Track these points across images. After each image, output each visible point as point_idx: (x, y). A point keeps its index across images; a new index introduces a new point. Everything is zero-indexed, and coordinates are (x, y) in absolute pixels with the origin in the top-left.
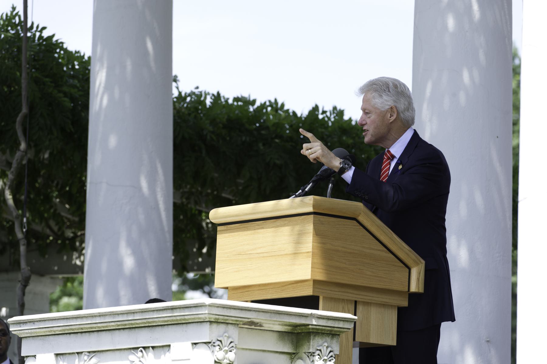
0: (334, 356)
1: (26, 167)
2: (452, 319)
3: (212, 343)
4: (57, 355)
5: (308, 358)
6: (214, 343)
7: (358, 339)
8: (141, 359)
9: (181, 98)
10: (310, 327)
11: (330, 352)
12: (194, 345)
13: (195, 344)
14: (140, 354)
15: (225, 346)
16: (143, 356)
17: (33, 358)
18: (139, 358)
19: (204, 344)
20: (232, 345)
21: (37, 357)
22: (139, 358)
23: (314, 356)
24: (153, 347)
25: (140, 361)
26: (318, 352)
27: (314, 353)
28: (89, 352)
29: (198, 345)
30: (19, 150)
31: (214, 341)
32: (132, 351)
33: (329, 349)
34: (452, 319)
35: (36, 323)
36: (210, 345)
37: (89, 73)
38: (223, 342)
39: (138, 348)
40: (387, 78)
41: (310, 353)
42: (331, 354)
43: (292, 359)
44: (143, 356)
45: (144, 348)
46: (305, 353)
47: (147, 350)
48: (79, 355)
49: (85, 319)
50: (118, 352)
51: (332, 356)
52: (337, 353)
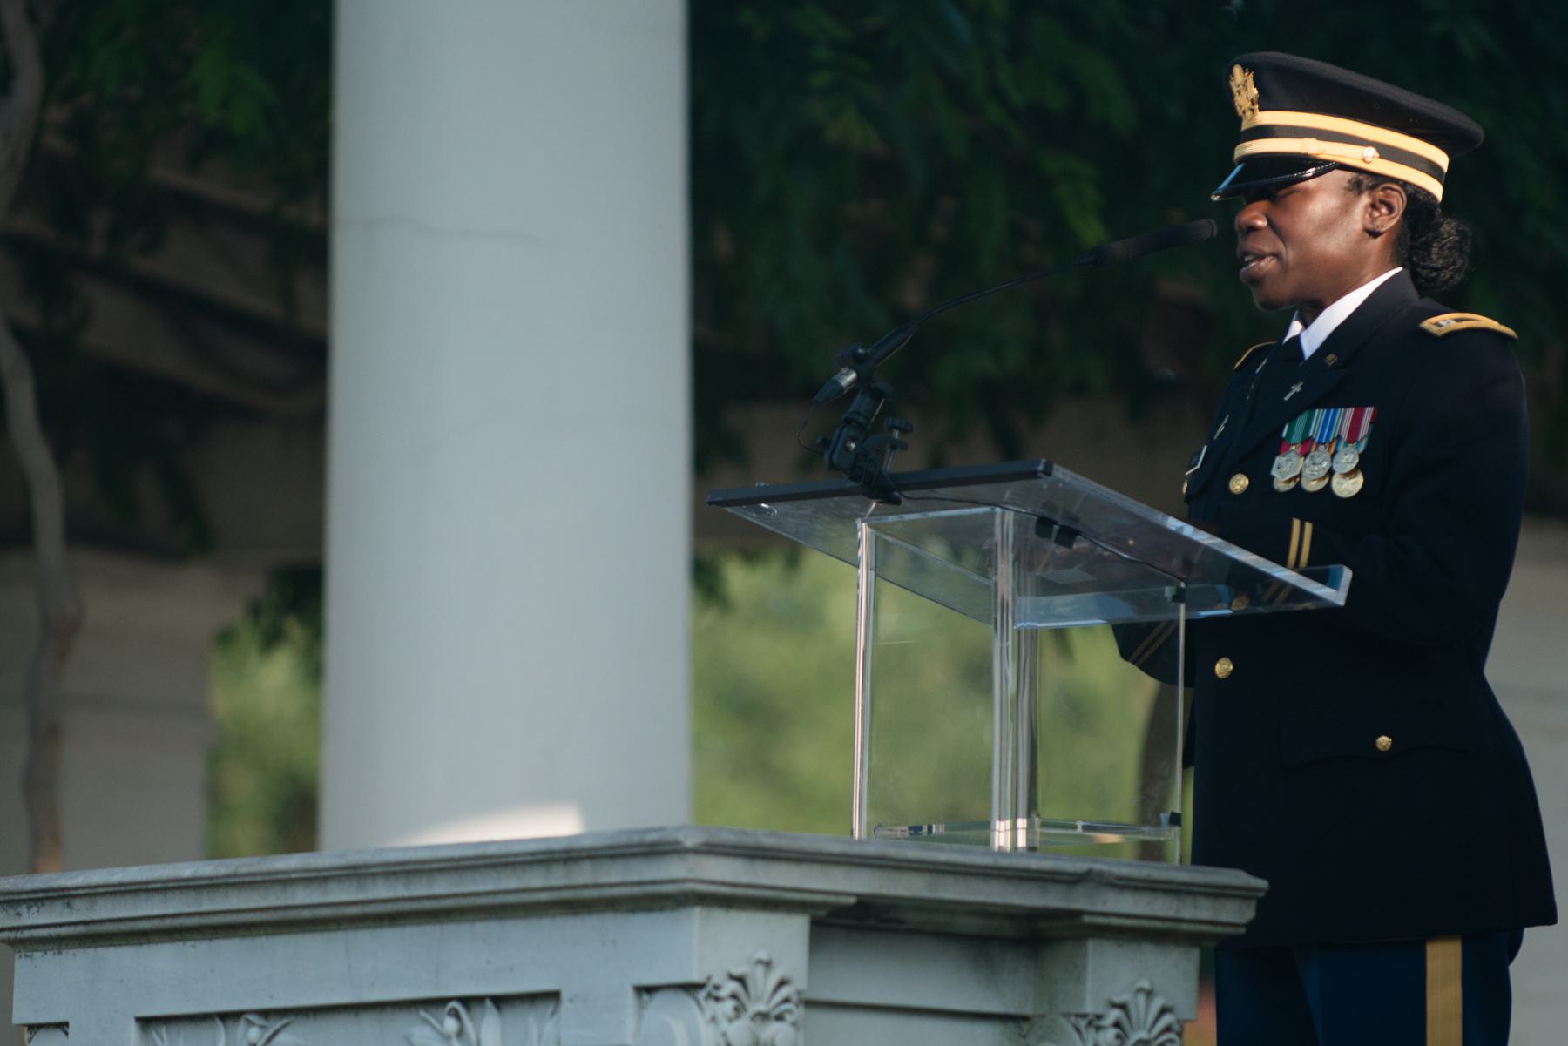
2: (1547, 916)
3: (709, 988)
4: (146, 1023)
5: (1076, 1035)
6: (717, 987)
9: (1287, 450)
10: (1087, 919)
11: (1164, 1011)
12: (646, 997)
13: (650, 990)
14: (451, 1024)
15: (758, 999)
16: (461, 1033)
17: (59, 1034)
19: (684, 999)
20: (785, 992)
21: (70, 1031)
23: (1098, 1029)
24: (500, 1001)
26: (1115, 1014)
27: (1099, 1017)
28: (265, 1014)
29: (659, 997)
30: (1070, 546)
31: (715, 981)
32: (423, 1013)
33: (1158, 1003)
34: (1547, 916)
35: (77, 903)
36: (702, 994)
37: (305, 251)
38: (750, 984)
39: (441, 1002)
41: (1084, 1016)
44: (461, 1033)
45: (467, 1001)
46: (1067, 1015)
47: (476, 1010)
48: (230, 1023)
50: (368, 1021)
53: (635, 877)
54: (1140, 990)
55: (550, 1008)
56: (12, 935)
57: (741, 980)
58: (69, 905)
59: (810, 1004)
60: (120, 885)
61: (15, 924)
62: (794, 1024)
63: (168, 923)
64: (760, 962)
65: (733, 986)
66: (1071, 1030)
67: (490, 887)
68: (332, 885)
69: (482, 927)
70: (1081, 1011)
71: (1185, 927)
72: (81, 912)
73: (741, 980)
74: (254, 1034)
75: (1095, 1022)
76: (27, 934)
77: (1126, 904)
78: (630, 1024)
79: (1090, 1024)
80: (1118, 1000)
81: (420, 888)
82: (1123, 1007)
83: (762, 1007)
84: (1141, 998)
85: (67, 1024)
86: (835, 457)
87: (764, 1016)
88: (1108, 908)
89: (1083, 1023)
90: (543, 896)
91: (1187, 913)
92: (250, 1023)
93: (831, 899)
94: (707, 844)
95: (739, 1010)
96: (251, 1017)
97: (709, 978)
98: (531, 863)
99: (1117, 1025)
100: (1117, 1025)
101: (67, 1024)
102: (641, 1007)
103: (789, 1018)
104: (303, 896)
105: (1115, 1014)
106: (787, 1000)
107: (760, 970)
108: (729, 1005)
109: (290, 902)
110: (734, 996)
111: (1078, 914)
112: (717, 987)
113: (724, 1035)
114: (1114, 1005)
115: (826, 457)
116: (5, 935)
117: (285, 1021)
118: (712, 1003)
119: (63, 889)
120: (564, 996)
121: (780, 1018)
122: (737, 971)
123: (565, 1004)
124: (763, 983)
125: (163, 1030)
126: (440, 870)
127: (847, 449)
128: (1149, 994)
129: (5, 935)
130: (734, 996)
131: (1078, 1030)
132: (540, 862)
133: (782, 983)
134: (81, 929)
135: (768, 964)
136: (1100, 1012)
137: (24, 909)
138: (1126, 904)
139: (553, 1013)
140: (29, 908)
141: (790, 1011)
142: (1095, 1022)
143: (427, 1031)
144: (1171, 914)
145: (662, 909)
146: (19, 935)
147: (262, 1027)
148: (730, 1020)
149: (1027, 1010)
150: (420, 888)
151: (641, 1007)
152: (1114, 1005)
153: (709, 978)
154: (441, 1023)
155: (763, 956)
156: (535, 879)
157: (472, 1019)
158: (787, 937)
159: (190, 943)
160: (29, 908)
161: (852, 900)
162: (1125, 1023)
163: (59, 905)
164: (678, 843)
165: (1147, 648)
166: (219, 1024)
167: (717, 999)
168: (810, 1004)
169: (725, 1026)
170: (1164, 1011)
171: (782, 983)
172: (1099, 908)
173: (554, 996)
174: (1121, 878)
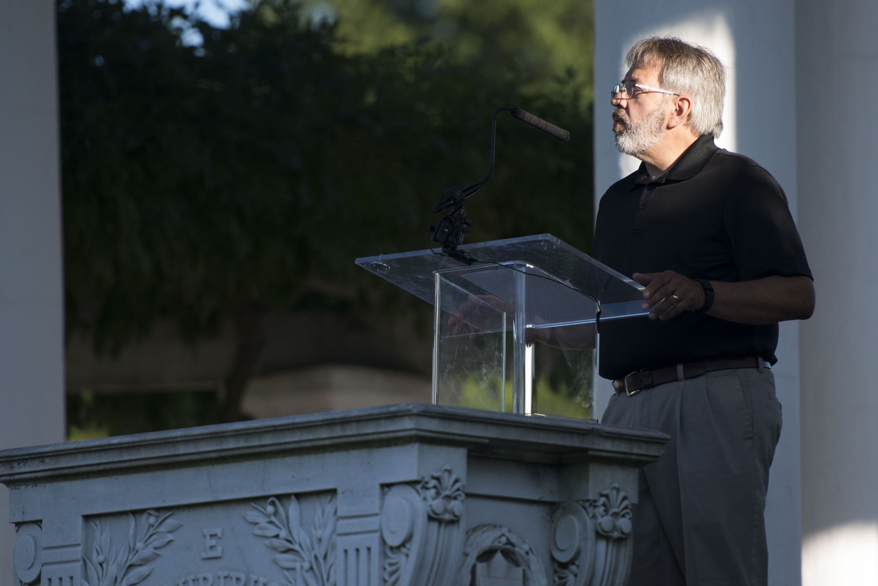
0: (630, 507)
1: (447, 281)
4: (87, 518)
6: (427, 483)
7: (519, 571)
8: (273, 519)
10: (591, 453)
11: (625, 498)
12: (386, 489)
13: (389, 486)
14: (270, 509)
15: (446, 489)
16: (276, 513)
17: (36, 527)
18: (268, 516)
19: (410, 492)
20: (458, 485)
21: (43, 525)
22: (268, 516)
23: (595, 507)
24: (299, 496)
25: (271, 522)
26: (603, 500)
27: (595, 501)
28: (158, 510)
29: (394, 489)
31: (426, 479)
32: (253, 504)
33: (622, 494)
35: (47, 460)
36: (419, 487)
38: (442, 481)
39: (265, 498)
40: (778, 185)
41: (588, 501)
42: (626, 503)
43: (552, 514)
44: (276, 513)
45: (280, 497)
46: (578, 501)
49: (80, 457)
50: (220, 512)
51: (626, 508)
52: (636, 501)
53: (382, 429)
54: (614, 488)
55: (329, 498)
56: (8, 478)
57: (438, 479)
58: (42, 461)
59: (469, 495)
60: (61, 451)
61: (11, 472)
62: (462, 501)
63: (102, 467)
64: (446, 470)
65: (433, 482)
66: (581, 508)
67: (296, 439)
68: (383, 422)
69: (289, 460)
70: (585, 498)
71: (634, 457)
72: (50, 464)
73: (438, 479)
74: (152, 520)
75: (593, 504)
76: (17, 477)
77: (608, 445)
78: (377, 502)
79: (590, 505)
80: (604, 492)
81: (255, 442)
82: (607, 496)
83: (448, 493)
84: (614, 492)
85: (41, 521)
86: (437, 236)
87: (448, 498)
88: (601, 447)
89: (587, 504)
90: (327, 442)
91: (635, 451)
92: (150, 514)
93: (478, 440)
94: (424, 411)
95: (438, 494)
96: (151, 512)
97: (423, 478)
98: (321, 426)
99: (604, 505)
100: (604, 505)
101: (41, 521)
102: (383, 495)
103: (460, 498)
104: (182, 449)
105: (603, 500)
106: (458, 490)
107: (446, 475)
108: (432, 492)
109: (176, 453)
110: (435, 487)
111: (586, 450)
112: (427, 483)
113: (431, 506)
114: (602, 495)
115: (432, 236)
116: (4, 478)
117: (170, 513)
118: (424, 491)
119: (40, 453)
120: (339, 491)
121: (455, 498)
122: (436, 474)
123: (340, 496)
124: (448, 481)
125: (97, 522)
126: (266, 432)
127: (443, 232)
128: (618, 490)
129: (4, 478)
130: (435, 487)
131: (585, 509)
132: (327, 425)
133: (456, 481)
134: (49, 473)
135: (449, 472)
136: (595, 498)
137: (16, 464)
138: (608, 445)
139: (330, 501)
140: (19, 464)
141: (460, 495)
142: (593, 504)
143: (256, 513)
144: (628, 451)
145: (396, 445)
146: (12, 478)
147: (156, 517)
148: (434, 499)
149: (555, 499)
150: (255, 442)
151: (383, 495)
152: (602, 495)
153: (423, 478)
154: (265, 510)
155: (448, 467)
156: (324, 433)
157: (283, 506)
158: (455, 460)
159: (114, 477)
160: (19, 464)
161: (486, 441)
162: (607, 504)
163: (37, 462)
164: (410, 411)
165: (173, 442)
166: (131, 515)
167: (427, 489)
168: (469, 495)
169: (430, 502)
170: (625, 498)
171: (456, 481)
172: (596, 447)
173: (333, 492)
174: (607, 433)
